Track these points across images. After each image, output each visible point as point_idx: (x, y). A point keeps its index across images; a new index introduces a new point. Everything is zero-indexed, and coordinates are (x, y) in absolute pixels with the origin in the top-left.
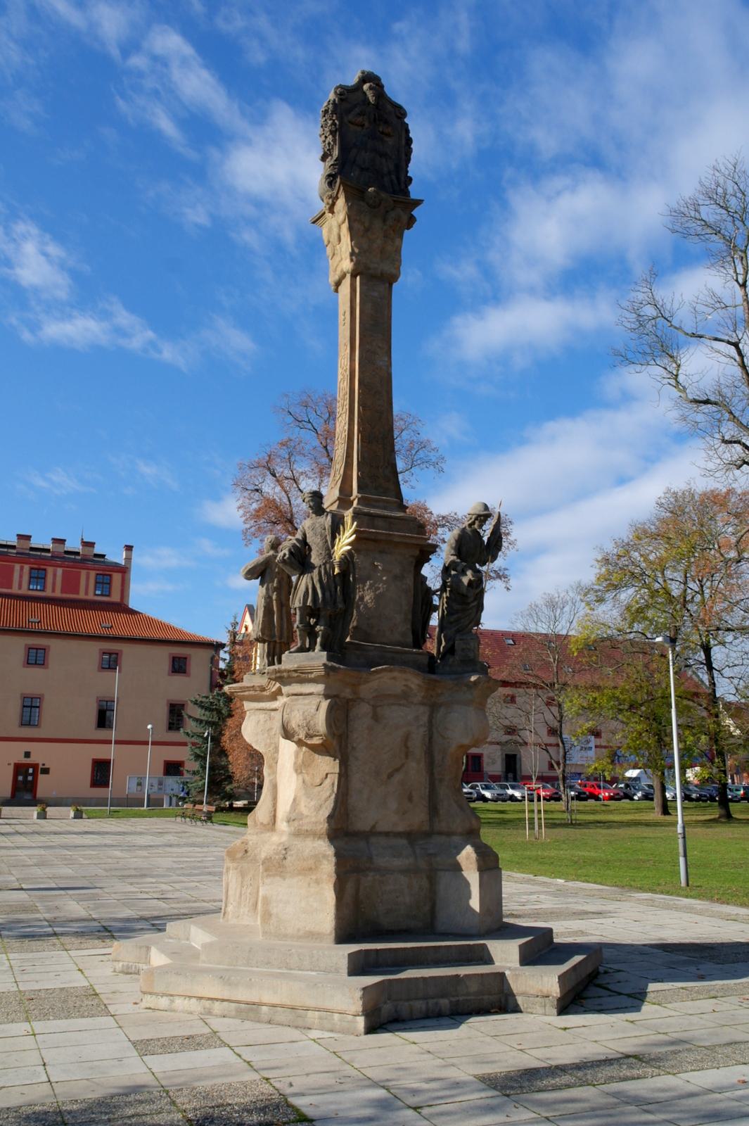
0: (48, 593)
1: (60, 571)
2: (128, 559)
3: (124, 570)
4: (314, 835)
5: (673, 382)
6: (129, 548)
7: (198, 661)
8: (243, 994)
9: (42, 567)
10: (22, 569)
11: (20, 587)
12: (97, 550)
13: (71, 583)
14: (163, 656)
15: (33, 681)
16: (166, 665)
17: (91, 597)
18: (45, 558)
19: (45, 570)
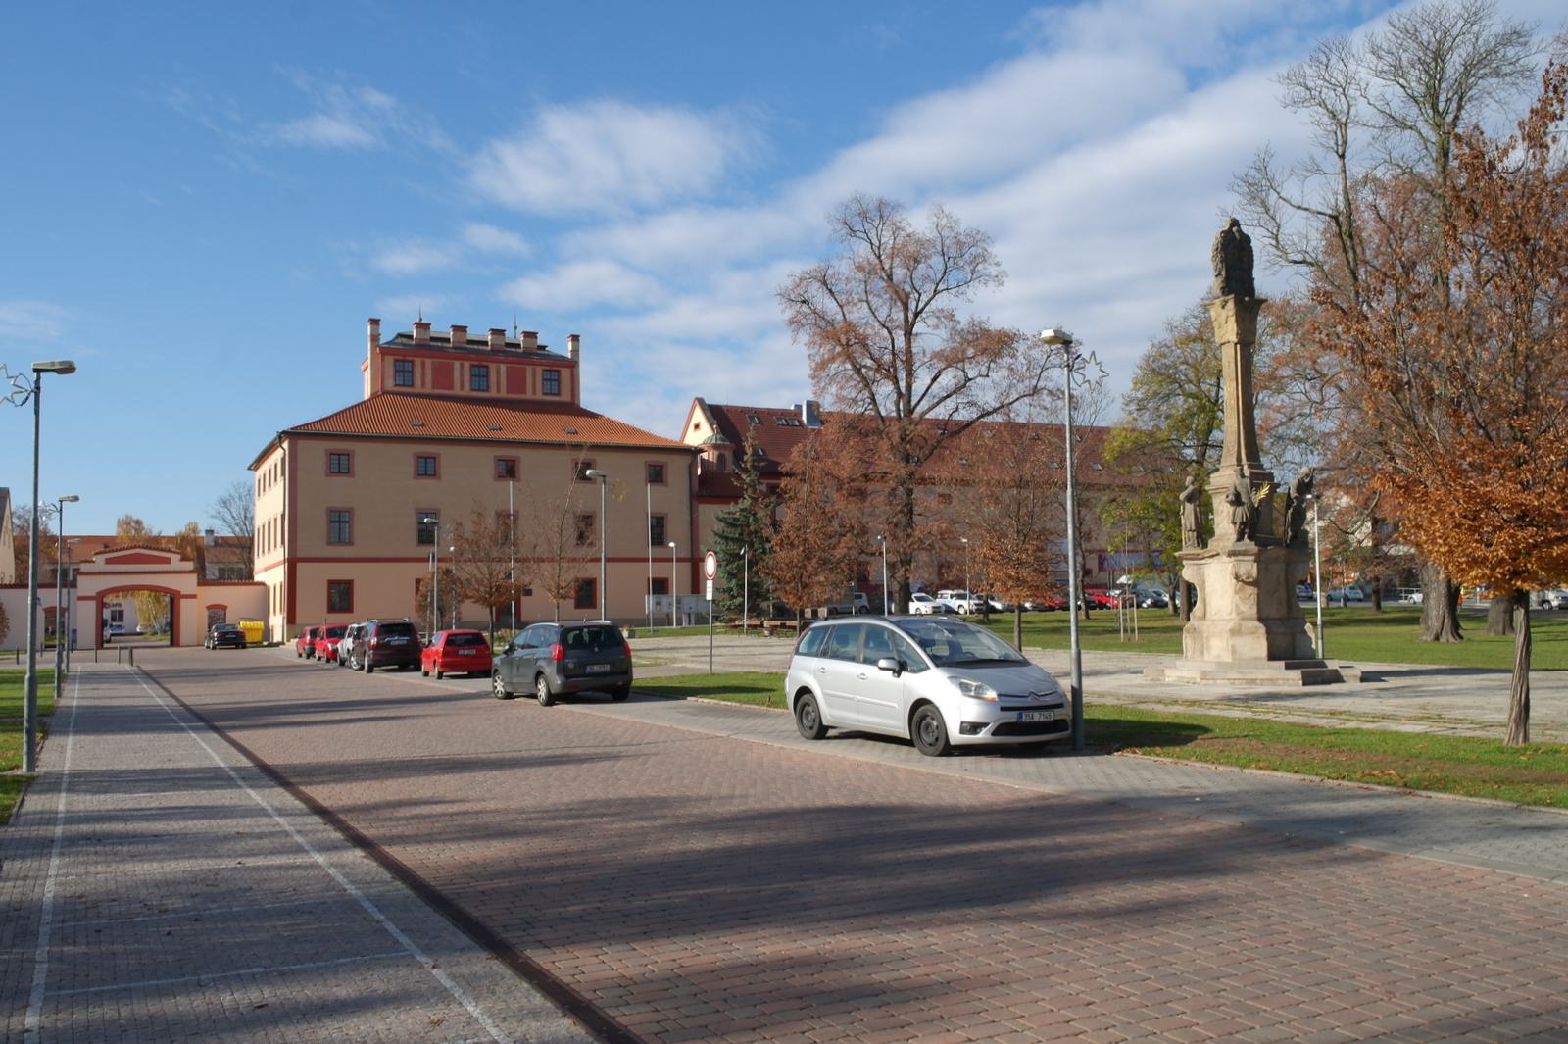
0: (493, 393)
1: (503, 368)
2: (575, 351)
3: (572, 364)
4: (1252, 619)
5: (1274, 242)
6: (575, 338)
7: (676, 468)
8: (1249, 677)
9: (484, 363)
10: (462, 366)
11: (462, 387)
12: (540, 341)
13: (516, 381)
14: (638, 464)
15: (581, 498)
16: (642, 474)
17: (539, 396)
18: (484, 352)
19: (558, 371)
